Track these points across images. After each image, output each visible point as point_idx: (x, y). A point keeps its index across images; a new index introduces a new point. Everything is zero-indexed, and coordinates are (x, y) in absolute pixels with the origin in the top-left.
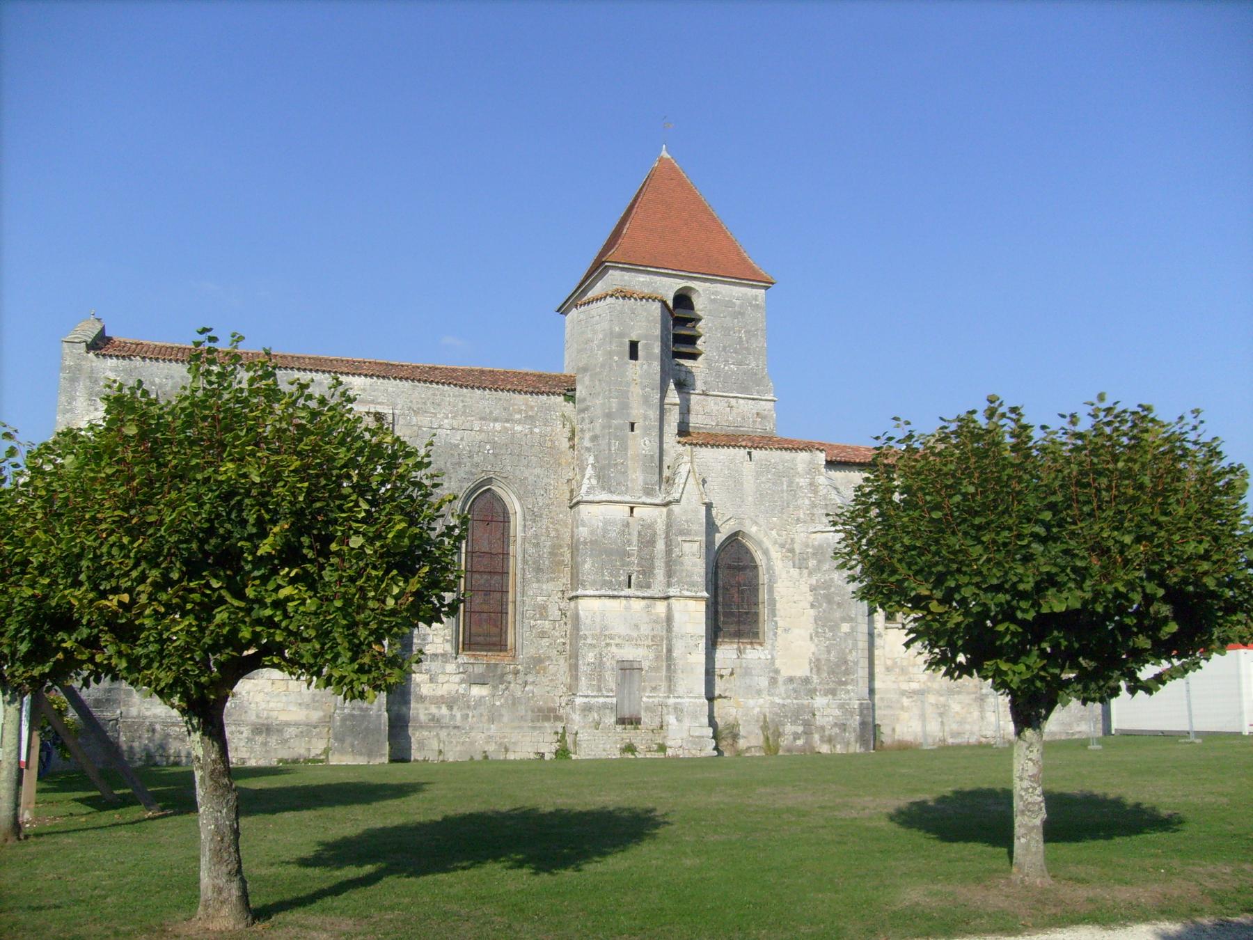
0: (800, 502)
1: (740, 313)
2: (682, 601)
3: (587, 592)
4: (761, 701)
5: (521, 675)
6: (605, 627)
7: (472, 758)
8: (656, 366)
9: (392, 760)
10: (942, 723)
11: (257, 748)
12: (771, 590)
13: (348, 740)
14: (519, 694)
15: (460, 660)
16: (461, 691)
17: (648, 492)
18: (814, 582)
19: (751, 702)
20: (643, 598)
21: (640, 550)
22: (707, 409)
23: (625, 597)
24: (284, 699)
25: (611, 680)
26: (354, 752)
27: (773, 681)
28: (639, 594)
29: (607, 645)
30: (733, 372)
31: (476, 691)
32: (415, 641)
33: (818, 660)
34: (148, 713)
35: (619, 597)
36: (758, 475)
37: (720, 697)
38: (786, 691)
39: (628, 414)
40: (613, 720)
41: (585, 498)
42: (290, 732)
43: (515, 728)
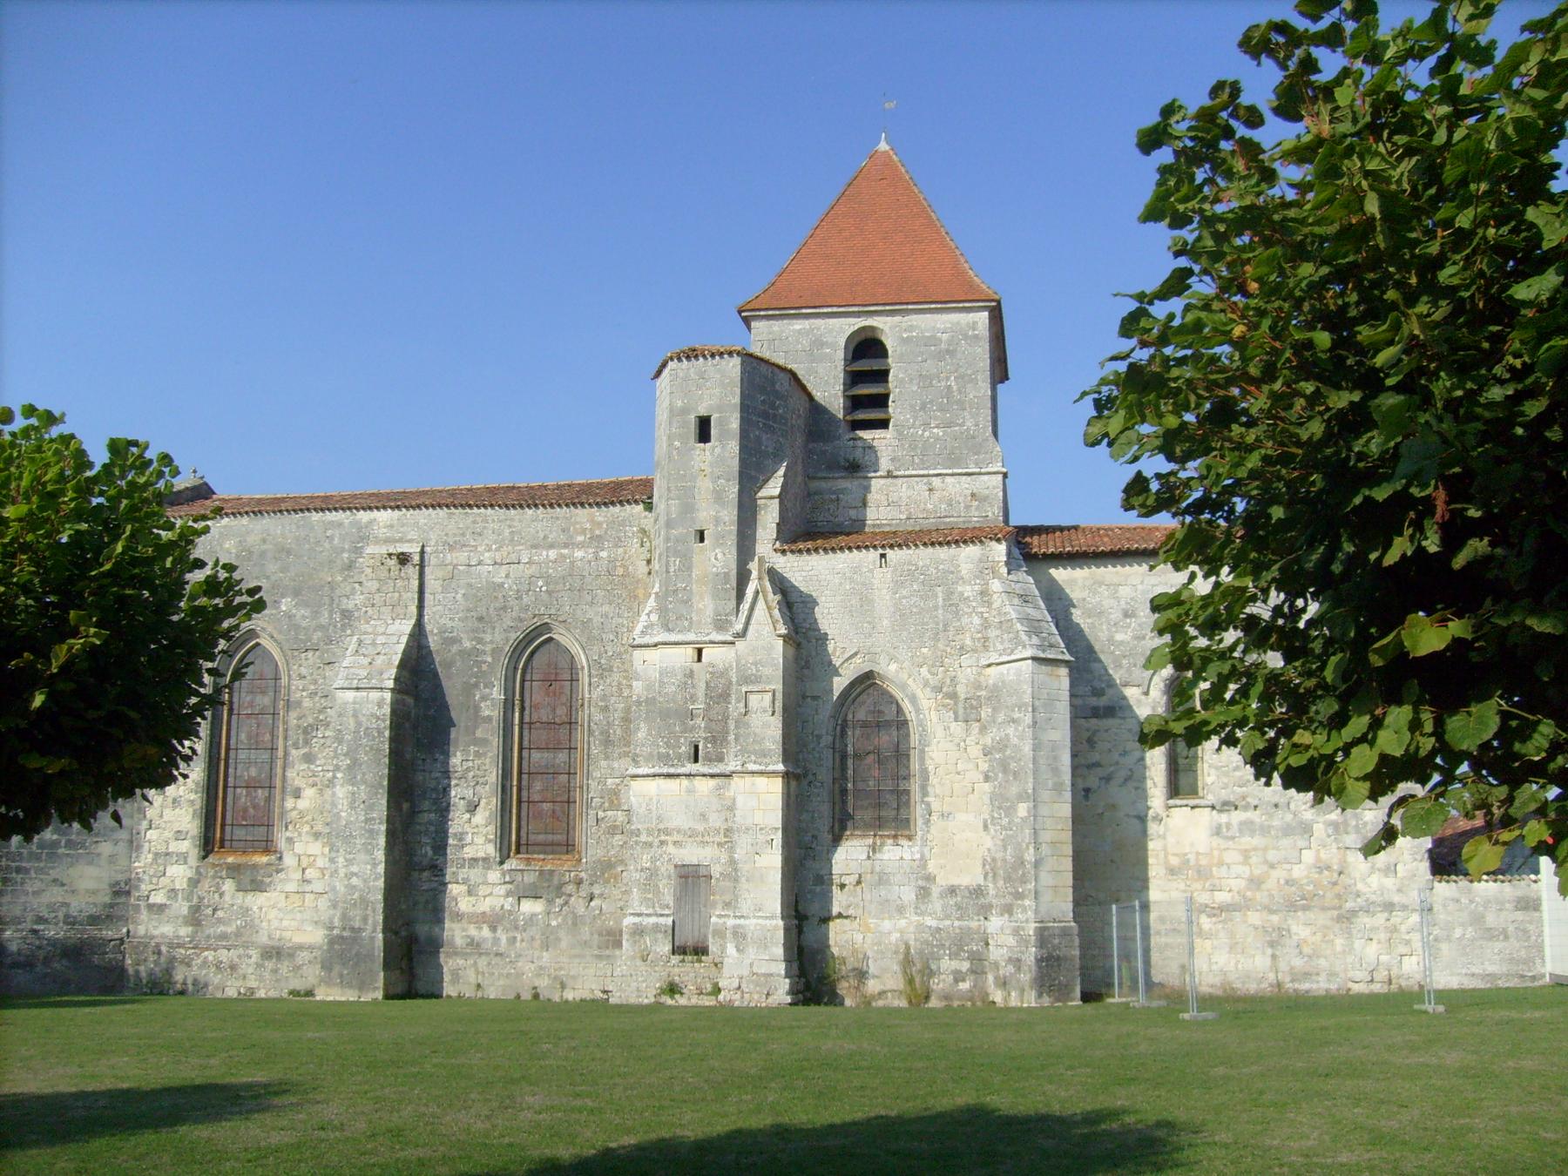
0: (965, 620)
1: (948, 351)
2: (748, 779)
3: (640, 771)
4: (903, 923)
5: (584, 886)
6: (660, 819)
7: (518, 997)
8: (734, 447)
9: (387, 997)
10: (1274, 957)
11: (267, 975)
12: (922, 760)
13: (337, 969)
14: (581, 910)
15: (506, 866)
16: (507, 907)
17: (721, 625)
18: (989, 741)
19: (887, 925)
20: (712, 776)
21: (708, 708)
22: (894, 497)
23: (689, 775)
24: (299, 916)
25: (667, 891)
26: (344, 983)
27: (924, 893)
28: (706, 770)
29: (662, 843)
30: (938, 439)
31: (529, 907)
32: (451, 841)
33: (994, 860)
34: (156, 933)
35: (678, 775)
36: (898, 585)
37: (840, 916)
38: (944, 907)
39: (693, 520)
40: (668, 948)
41: (638, 641)
42: (304, 956)
43: (576, 956)
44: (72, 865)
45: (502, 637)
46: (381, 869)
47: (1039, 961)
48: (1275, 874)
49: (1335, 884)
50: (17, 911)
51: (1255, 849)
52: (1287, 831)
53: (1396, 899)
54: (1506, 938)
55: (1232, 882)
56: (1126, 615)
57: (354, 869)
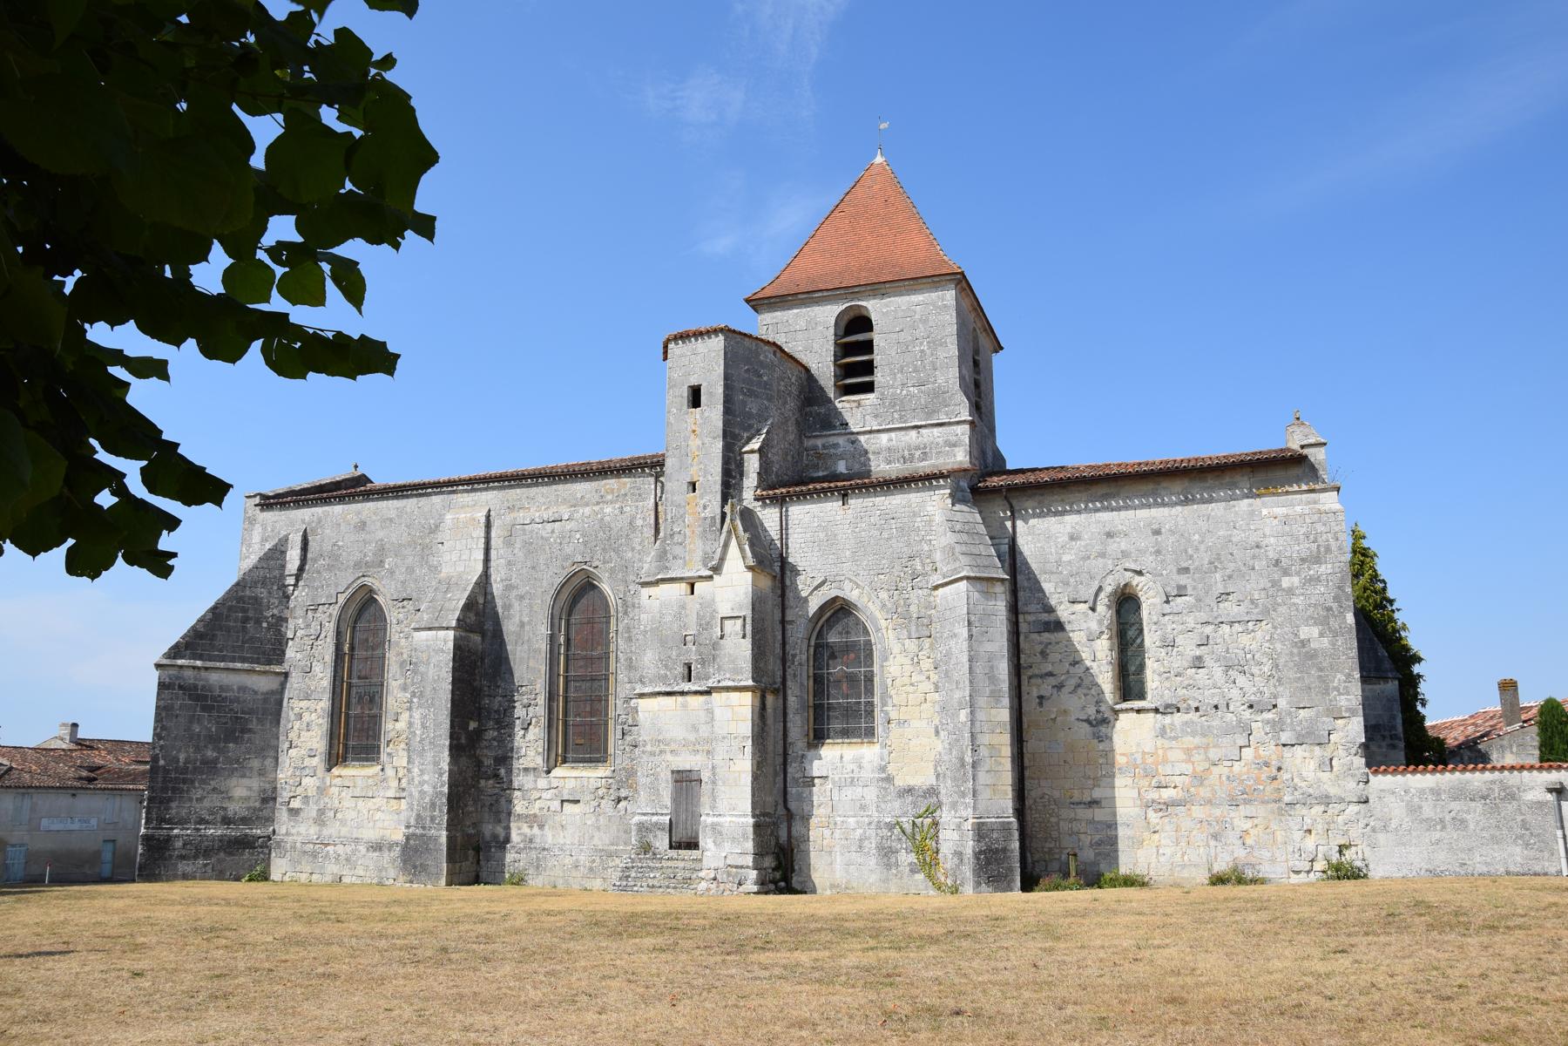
3: (647, 690)
6: (660, 731)
23: (682, 693)
44: (229, 776)
45: (552, 577)
46: (445, 777)
47: (977, 855)
49: (1275, 779)
50: (184, 812)
51: (1197, 748)
52: (1228, 731)
55: (1178, 780)
56: (1072, 538)
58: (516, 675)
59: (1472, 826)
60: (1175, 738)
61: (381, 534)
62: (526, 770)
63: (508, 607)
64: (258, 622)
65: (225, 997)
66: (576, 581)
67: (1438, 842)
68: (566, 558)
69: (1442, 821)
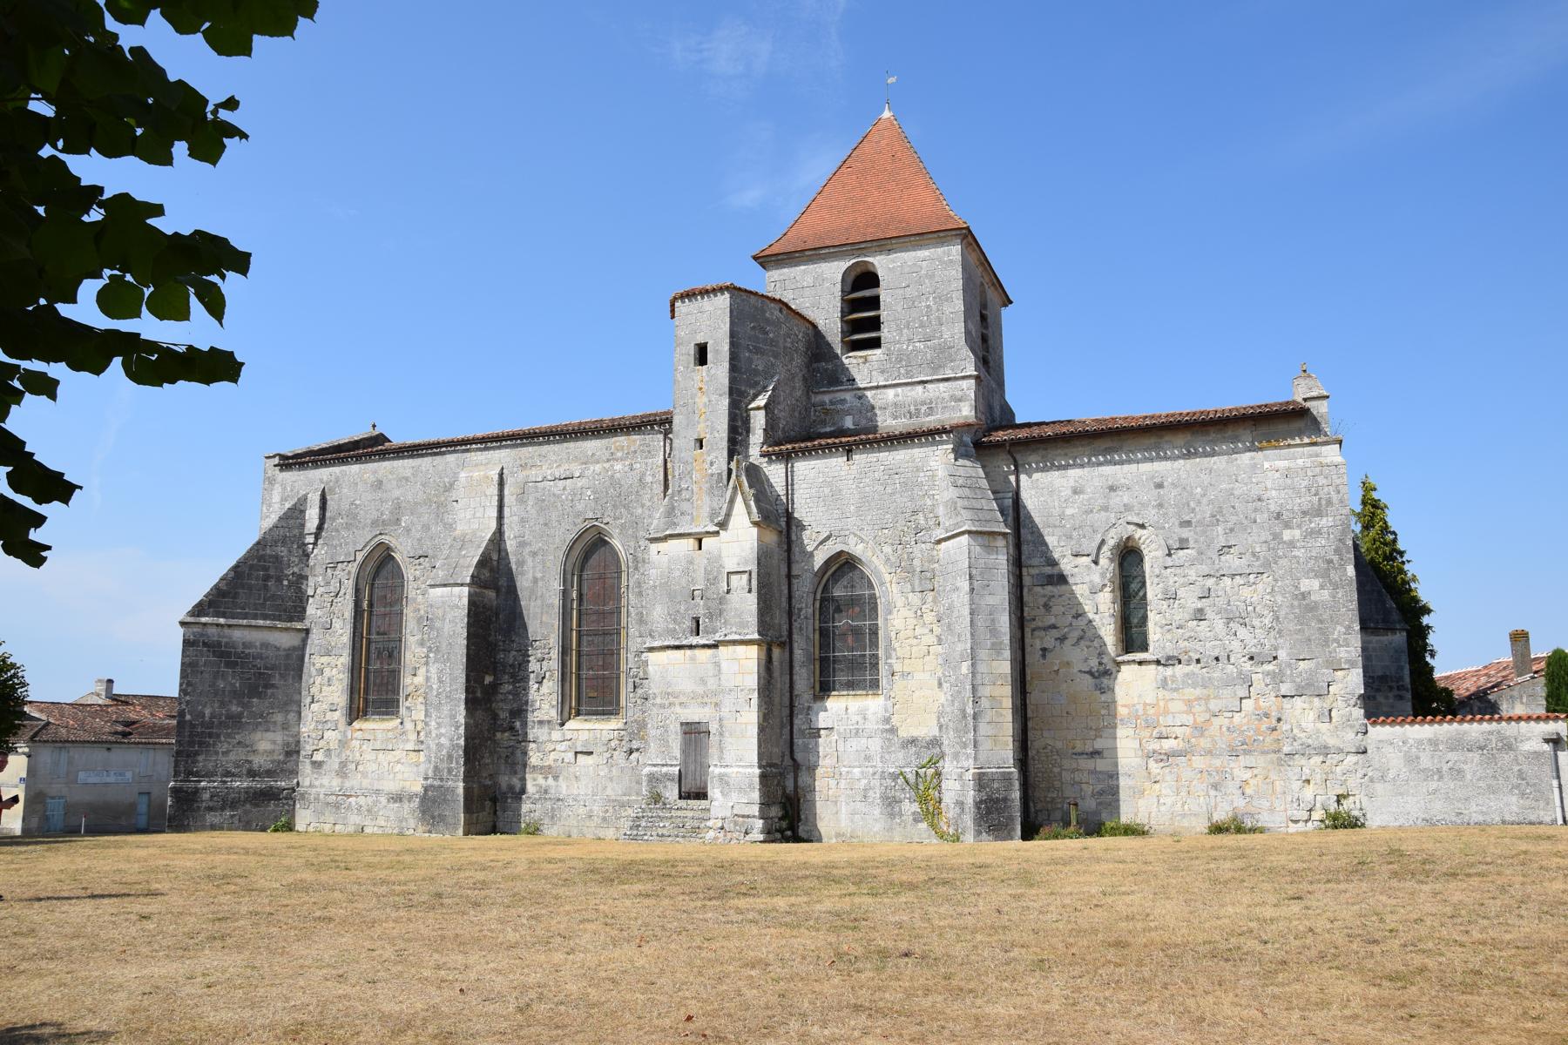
3: (656, 644)
6: (669, 684)
23: (691, 647)
28: (704, 641)
45: (564, 533)
46: (462, 730)
47: (978, 805)
48: (1216, 722)
49: (1274, 729)
50: (210, 766)
52: (1228, 683)
53: (1332, 742)
54: (1441, 778)
56: (1075, 492)
57: (443, 731)
58: (530, 630)
59: (1469, 777)
60: (1176, 690)
61: (397, 493)
62: (541, 722)
63: (521, 563)
64: (279, 580)
65: (223, 938)
66: (588, 537)
67: (1435, 791)
68: (578, 515)
69: (1439, 771)
